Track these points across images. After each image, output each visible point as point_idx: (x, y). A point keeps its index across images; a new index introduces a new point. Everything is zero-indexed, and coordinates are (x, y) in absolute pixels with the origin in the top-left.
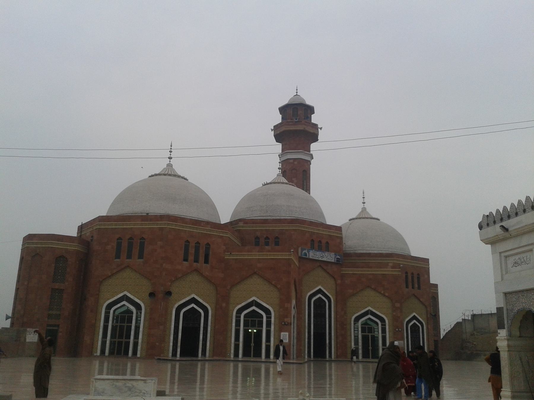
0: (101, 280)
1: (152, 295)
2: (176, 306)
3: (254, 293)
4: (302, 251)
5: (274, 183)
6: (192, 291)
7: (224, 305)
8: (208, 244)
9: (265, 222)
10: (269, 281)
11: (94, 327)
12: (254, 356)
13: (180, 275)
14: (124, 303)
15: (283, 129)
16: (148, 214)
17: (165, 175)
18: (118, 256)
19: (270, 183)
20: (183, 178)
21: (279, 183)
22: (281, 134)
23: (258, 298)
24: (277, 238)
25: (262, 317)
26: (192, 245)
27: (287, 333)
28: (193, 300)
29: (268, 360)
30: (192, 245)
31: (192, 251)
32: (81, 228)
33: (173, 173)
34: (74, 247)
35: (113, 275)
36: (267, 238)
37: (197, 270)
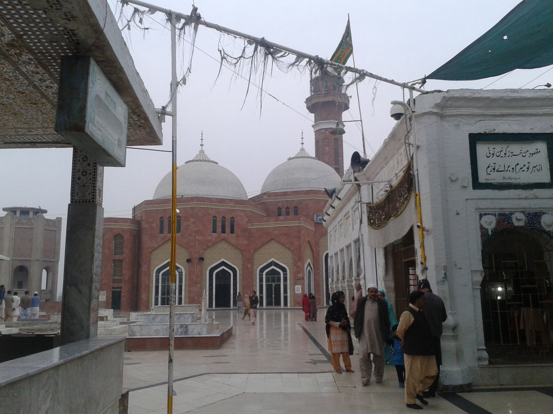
0: (150, 251)
1: (188, 261)
2: (209, 268)
3: (274, 255)
4: (317, 216)
5: (297, 158)
6: (222, 255)
7: (249, 266)
8: (232, 218)
9: (285, 194)
10: (283, 244)
11: (148, 287)
12: (275, 305)
13: (210, 244)
14: (273, 267)
15: (314, 101)
16: (182, 196)
17: (197, 161)
18: (161, 231)
19: (294, 158)
20: (212, 162)
21: (300, 157)
22: (313, 106)
23: (276, 259)
24: (296, 207)
25: (279, 274)
26: (219, 219)
27: (300, 286)
28: (223, 264)
29: (286, 307)
30: (219, 219)
31: (219, 224)
32: (134, 209)
33: (204, 159)
34: (128, 226)
35: (159, 246)
36: (287, 208)
37: (224, 239)
